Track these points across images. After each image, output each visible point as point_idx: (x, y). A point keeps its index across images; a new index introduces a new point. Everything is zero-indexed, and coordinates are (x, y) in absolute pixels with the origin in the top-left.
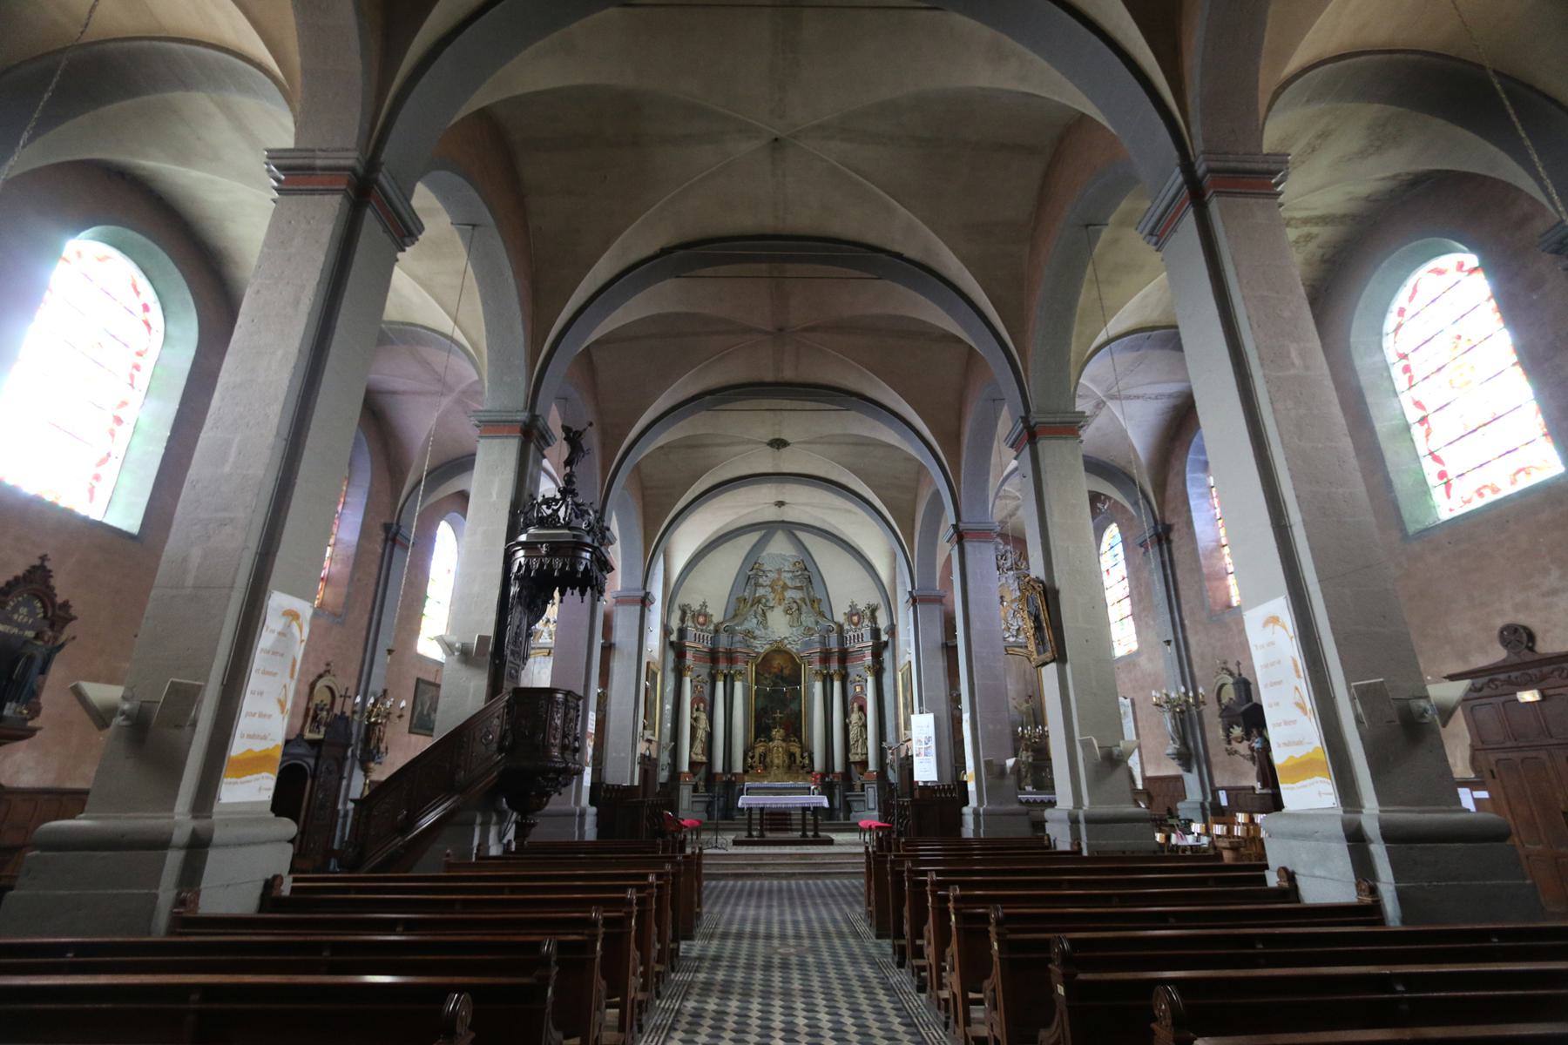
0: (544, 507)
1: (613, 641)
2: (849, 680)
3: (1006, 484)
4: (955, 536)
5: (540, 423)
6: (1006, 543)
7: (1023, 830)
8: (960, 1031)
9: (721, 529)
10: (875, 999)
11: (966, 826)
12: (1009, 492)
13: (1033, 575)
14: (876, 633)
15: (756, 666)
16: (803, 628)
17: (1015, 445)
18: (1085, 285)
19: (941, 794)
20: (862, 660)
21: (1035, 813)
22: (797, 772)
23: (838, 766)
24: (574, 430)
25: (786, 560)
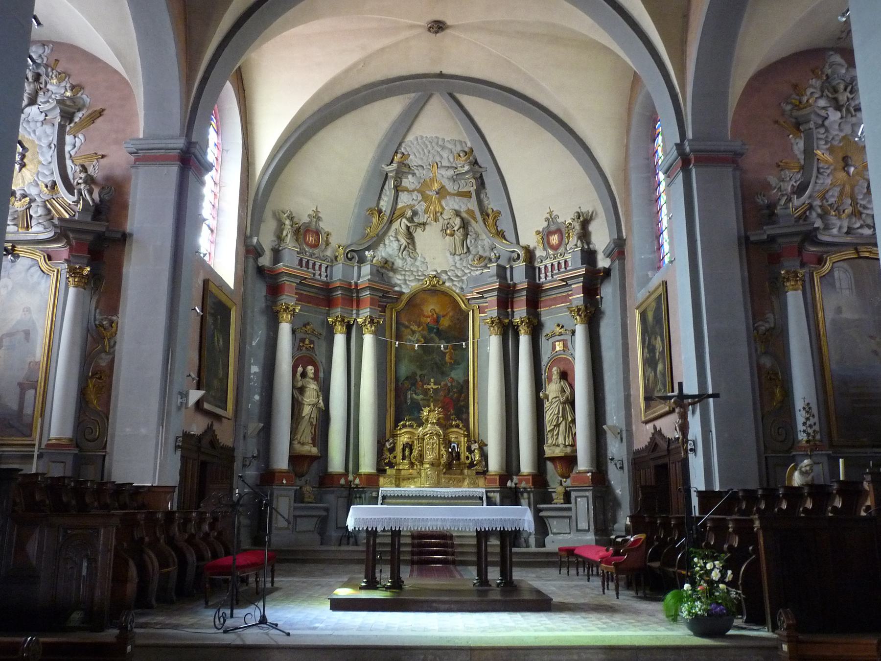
1: (129, 228)
14: (589, 256)
15: (398, 313)
16: (471, 257)
22: (462, 473)
23: (526, 465)
25: (443, 148)
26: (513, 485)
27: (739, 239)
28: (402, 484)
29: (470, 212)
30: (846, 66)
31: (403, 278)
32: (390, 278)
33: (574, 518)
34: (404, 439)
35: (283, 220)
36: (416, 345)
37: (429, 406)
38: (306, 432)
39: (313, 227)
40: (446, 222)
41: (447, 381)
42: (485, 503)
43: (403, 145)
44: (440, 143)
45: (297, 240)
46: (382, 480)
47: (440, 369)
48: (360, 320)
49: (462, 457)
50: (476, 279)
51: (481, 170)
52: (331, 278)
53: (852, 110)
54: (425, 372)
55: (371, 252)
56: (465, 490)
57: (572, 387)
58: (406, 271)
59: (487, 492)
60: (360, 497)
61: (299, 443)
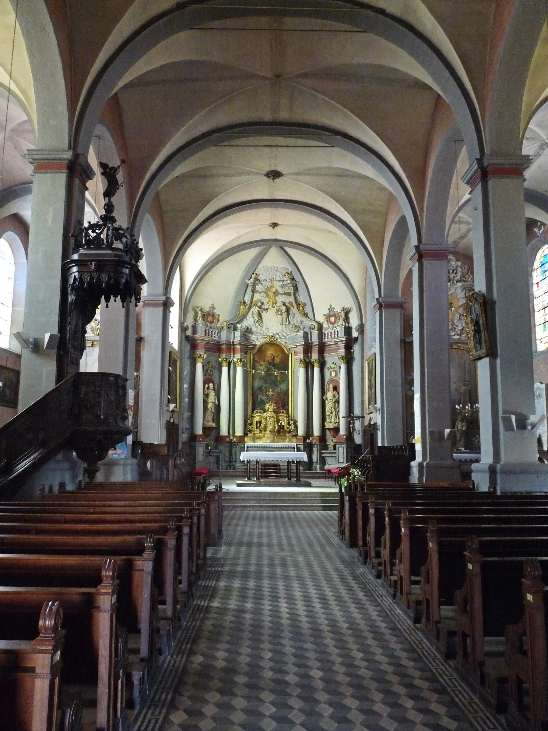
0: (90, 231)
1: (142, 335)
2: (326, 367)
3: (462, 211)
4: (417, 255)
5: (81, 160)
6: (458, 260)
7: (455, 479)
8: (404, 598)
9: (224, 246)
10: (328, 608)
11: (412, 475)
12: (463, 218)
13: (476, 290)
14: (348, 330)
15: (254, 355)
16: (291, 326)
17: (470, 182)
18: (539, 42)
19: (394, 452)
20: (337, 352)
21: (465, 468)
22: (285, 436)
23: (316, 432)
24: (110, 167)
25: (277, 271)
26: (310, 442)
27: (401, 341)
28: (256, 441)
29: (291, 303)
30: (455, 260)
31: (256, 337)
32: (250, 337)
33: (337, 457)
34: (256, 419)
35: (198, 312)
36: (263, 372)
37: (269, 403)
38: (209, 417)
39: (211, 312)
40: (278, 308)
41: (278, 390)
42: (296, 450)
43: (257, 270)
44: (275, 269)
45: (204, 320)
46: (246, 439)
47: (274, 383)
48: (235, 360)
49: (285, 428)
50: (293, 338)
51: (296, 282)
52: (220, 339)
53: (455, 282)
54: (267, 385)
55: (240, 325)
56: (286, 444)
57: (338, 394)
58: (258, 333)
59: (297, 445)
60: (236, 447)
61: (207, 421)
